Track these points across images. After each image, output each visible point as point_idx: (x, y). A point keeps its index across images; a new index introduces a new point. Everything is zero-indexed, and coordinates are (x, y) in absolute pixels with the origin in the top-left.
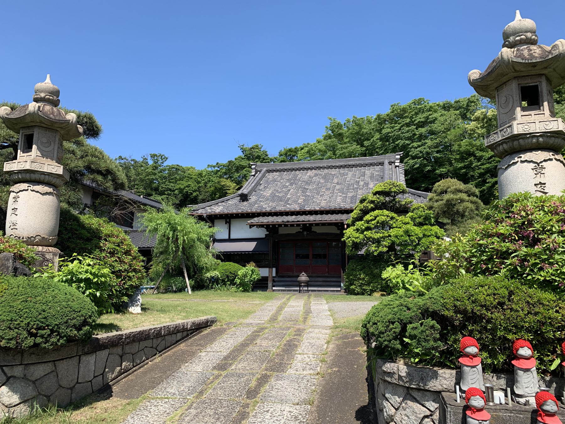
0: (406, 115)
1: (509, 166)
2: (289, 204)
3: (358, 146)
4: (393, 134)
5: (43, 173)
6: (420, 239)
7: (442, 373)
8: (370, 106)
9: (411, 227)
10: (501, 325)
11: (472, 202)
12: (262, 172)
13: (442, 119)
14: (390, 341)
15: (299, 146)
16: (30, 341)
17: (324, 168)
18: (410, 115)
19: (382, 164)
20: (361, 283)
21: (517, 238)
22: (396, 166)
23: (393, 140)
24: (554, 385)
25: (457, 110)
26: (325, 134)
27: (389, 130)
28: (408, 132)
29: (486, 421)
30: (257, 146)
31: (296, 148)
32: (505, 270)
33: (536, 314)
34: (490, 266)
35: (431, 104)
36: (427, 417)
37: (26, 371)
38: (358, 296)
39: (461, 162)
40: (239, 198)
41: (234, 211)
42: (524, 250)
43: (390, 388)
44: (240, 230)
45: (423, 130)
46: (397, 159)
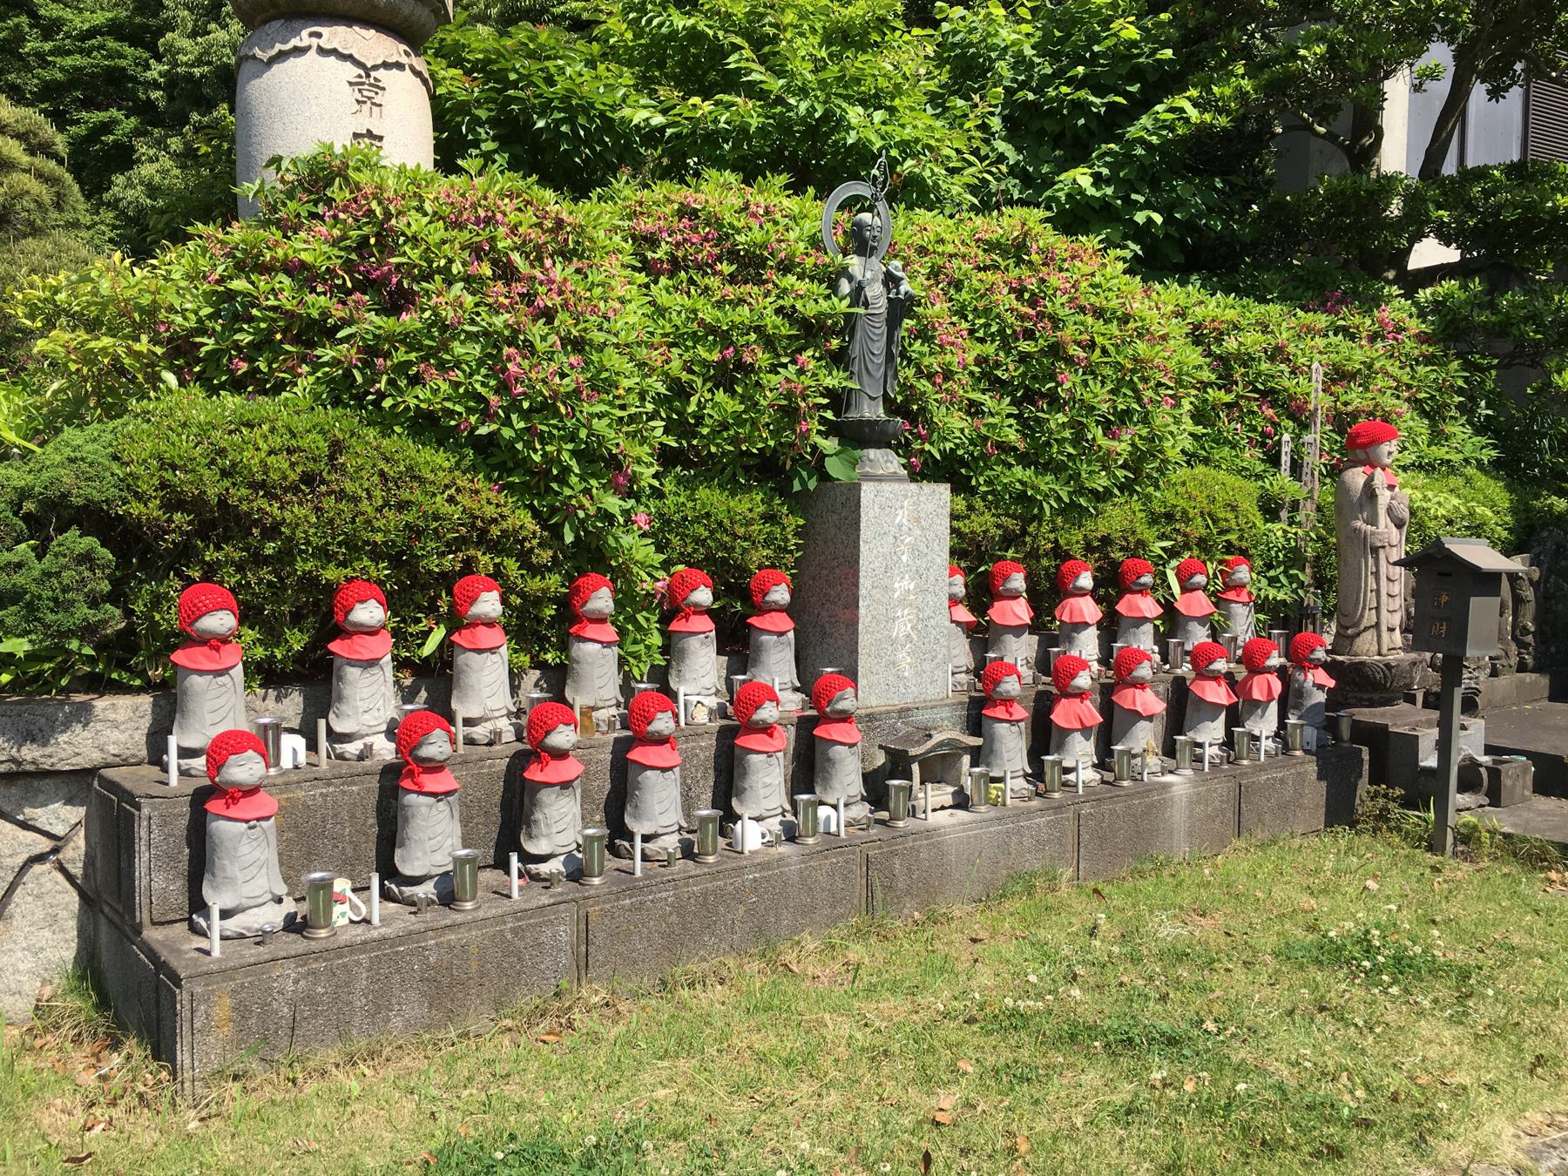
1: (282, 56)
7: (105, 709)
10: (308, 543)
11: (40, 175)
21: (349, 284)
24: (424, 694)
29: (267, 818)
32: (311, 379)
33: (403, 506)
34: (263, 366)
36: (40, 858)
37: (363, 123)
42: (374, 322)
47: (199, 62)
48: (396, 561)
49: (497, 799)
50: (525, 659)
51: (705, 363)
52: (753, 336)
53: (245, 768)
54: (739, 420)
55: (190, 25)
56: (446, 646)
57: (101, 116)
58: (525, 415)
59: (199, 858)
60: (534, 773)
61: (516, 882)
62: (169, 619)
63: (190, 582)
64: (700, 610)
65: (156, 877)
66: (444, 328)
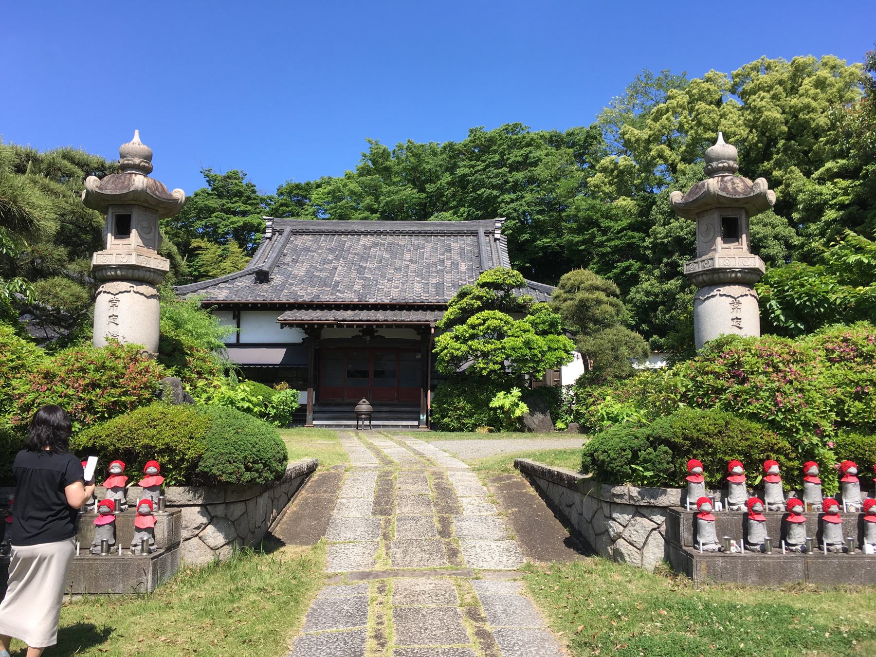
0: (495, 148)
1: (708, 298)
2: (339, 291)
3: (415, 191)
4: (473, 178)
5: (149, 270)
6: (543, 353)
8: (439, 125)
9: (531, 336)
11: (612, 304)
12: (285, 234)
13: (550, 162)
14: (622, 466)
15: (314, 179)
16: (248, 476)
17: (385, 233)
18: (501, 149)
19: (475, 234)
20: (460, 415)
22: (496, 240)
23: (473, 187)
25: (572, 147)
26: (361, 165)
27: (467, 171)
28: (497, 176)
30: (236, 173)
31: (307, 184)
33: (747, 440)
35: (532, 135)
36: (654, 529)
38: (453, 434)
39: (578, 234)
40: (253, 277)
41: (250, 299)
43: (619, 508)
44: (257, 329)
45: (519, 176)
46: (498, 228)
47: (667, 236)
48: (745, 455)
49: (779, 527)
50: (788, 487)
51: (849, 392)
52: (868, 383)
53: (706, 507)
54: (864, 411)
55: (662, 221)
56: (762, 481)
57: (626, 264)
58: (783, 413)
59: (696, 530)
60: (790, 519)
61: (784, 551)
62: (685, 468)
63: (690, 459)
64: (852, 475)
65: (685, 534)
66: (757, 388)
